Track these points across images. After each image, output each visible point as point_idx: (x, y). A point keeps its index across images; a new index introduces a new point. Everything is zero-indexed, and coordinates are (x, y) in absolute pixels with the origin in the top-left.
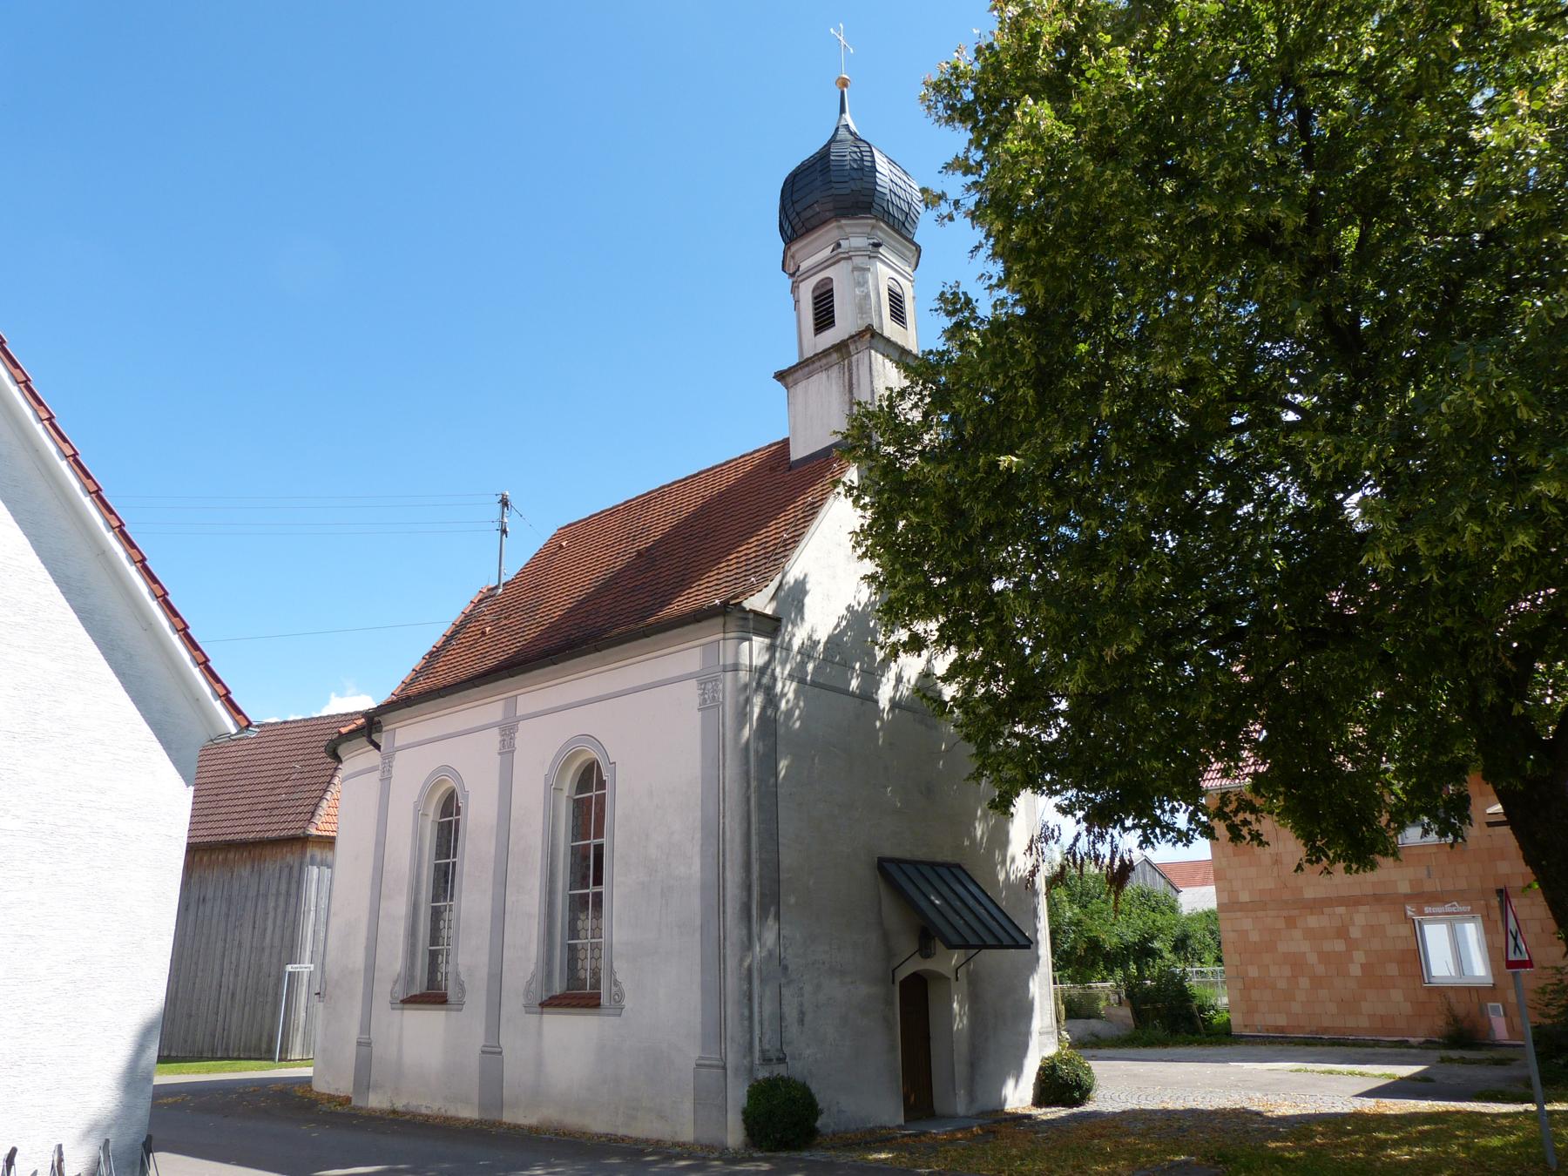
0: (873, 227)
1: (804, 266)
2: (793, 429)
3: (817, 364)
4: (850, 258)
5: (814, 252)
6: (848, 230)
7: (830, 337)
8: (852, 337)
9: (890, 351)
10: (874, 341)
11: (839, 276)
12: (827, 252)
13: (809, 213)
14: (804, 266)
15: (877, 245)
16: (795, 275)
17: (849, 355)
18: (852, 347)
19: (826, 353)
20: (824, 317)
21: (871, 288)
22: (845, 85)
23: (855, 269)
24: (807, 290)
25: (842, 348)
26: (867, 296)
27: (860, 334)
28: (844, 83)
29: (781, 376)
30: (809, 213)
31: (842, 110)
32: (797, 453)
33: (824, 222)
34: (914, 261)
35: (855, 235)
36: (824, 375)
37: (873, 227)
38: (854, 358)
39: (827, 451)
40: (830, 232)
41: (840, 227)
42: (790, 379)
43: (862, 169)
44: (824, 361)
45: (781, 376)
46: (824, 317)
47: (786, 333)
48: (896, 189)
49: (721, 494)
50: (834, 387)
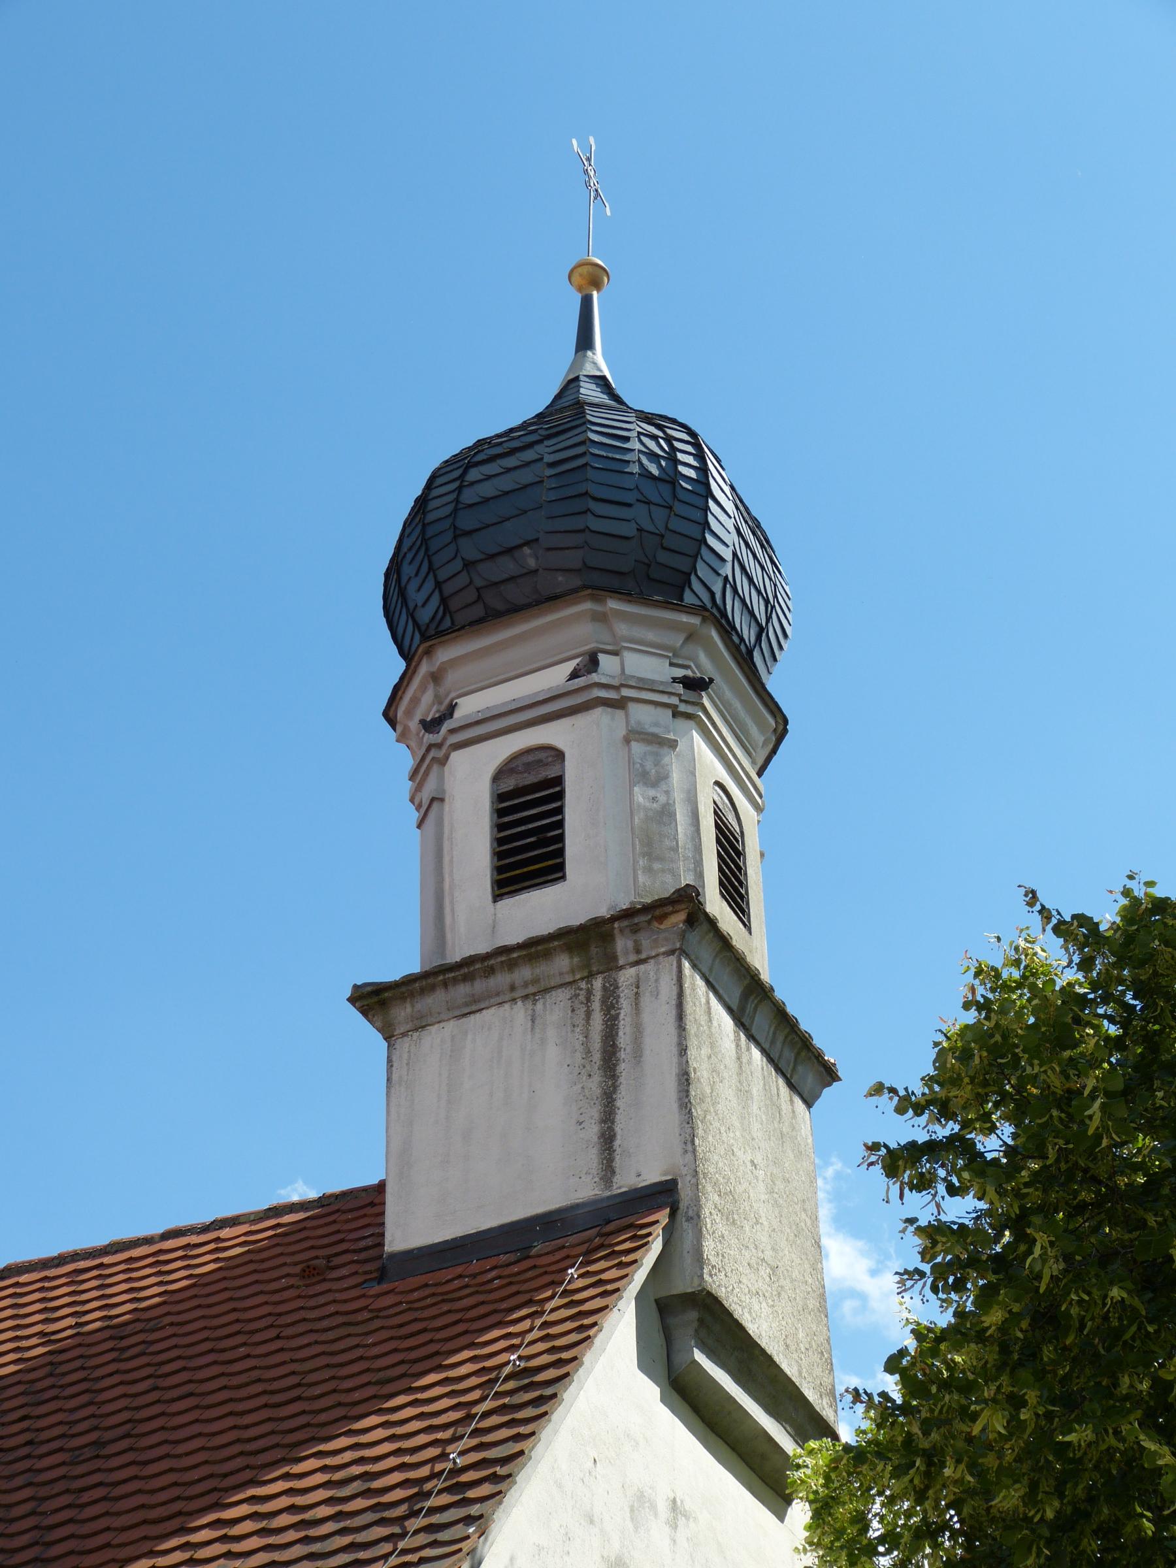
0: (691, 636)
1: (468, 707)
2: (401, 1153)
3: (502, 979)
4: (620, 704)
5: (509, 675)
6: (622, 629)
7: (540, 911)
8: (627, 914)
9: (725, 976)
10: (694, 937)
11: (586, 748)
12: (556, 677)
13: (507, 567)
14: (468, 707)
15: (696, 685)
16: (429, 730)
17: (611, 964)
18: (622, 945)
19: (535, 949)
20: (529, 841)
21: (678, 796)
22: (596, 284)
23: (634, 735)
24: (472, 778)
25: (590, 942)
26: (666, 814)
27: (657, 910)
28: (590, 278)
29: (373, 1000)
30: (507, 567)
31: (585, 341)
32: (408, 1229)
33: (553, 599)
34: (760, 762)
35: (642, 655)
36: (520, 1012)
37: (691, 636)
38: (626, 977)
39: (548, 1224)
40: (573, 626)
41: (601, 618)
42: (402, 1013)
43: (671, 478)
44: (525, 973)
45: (373, 1000)
46: (529, 841)
47: (387, 872)
48: (744, 554)
49: (115, 1332)
50: (553, 1052)
